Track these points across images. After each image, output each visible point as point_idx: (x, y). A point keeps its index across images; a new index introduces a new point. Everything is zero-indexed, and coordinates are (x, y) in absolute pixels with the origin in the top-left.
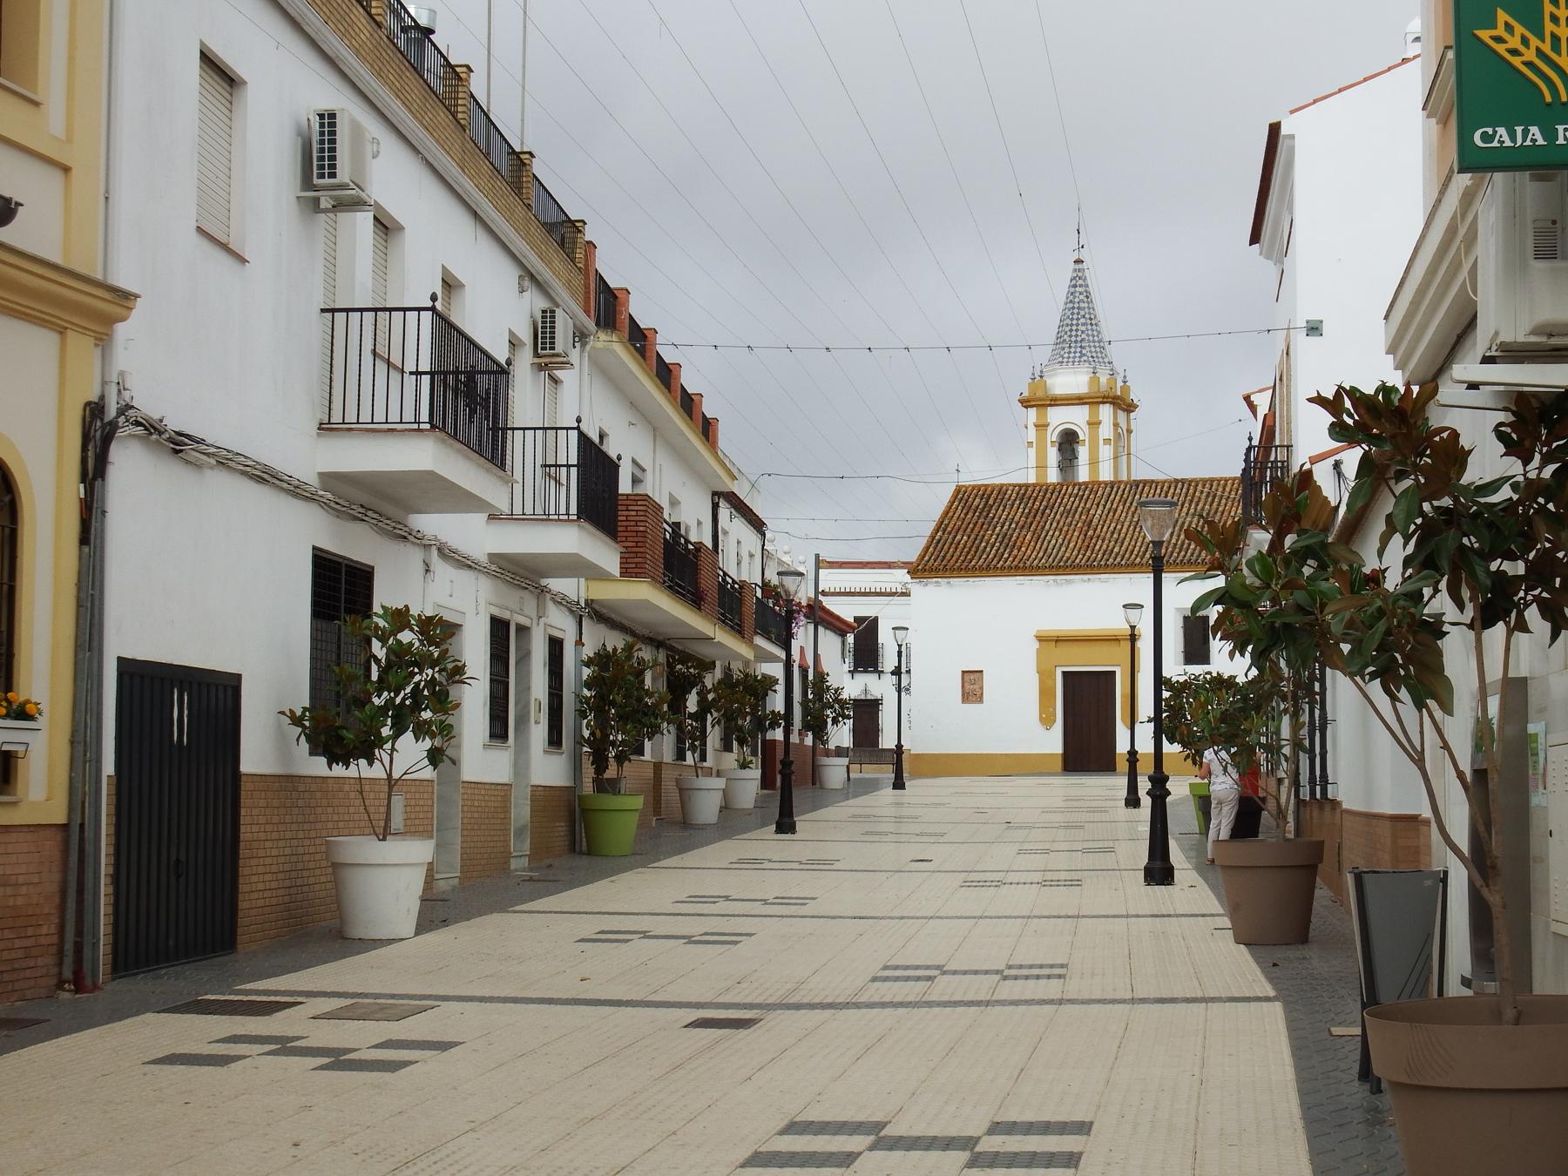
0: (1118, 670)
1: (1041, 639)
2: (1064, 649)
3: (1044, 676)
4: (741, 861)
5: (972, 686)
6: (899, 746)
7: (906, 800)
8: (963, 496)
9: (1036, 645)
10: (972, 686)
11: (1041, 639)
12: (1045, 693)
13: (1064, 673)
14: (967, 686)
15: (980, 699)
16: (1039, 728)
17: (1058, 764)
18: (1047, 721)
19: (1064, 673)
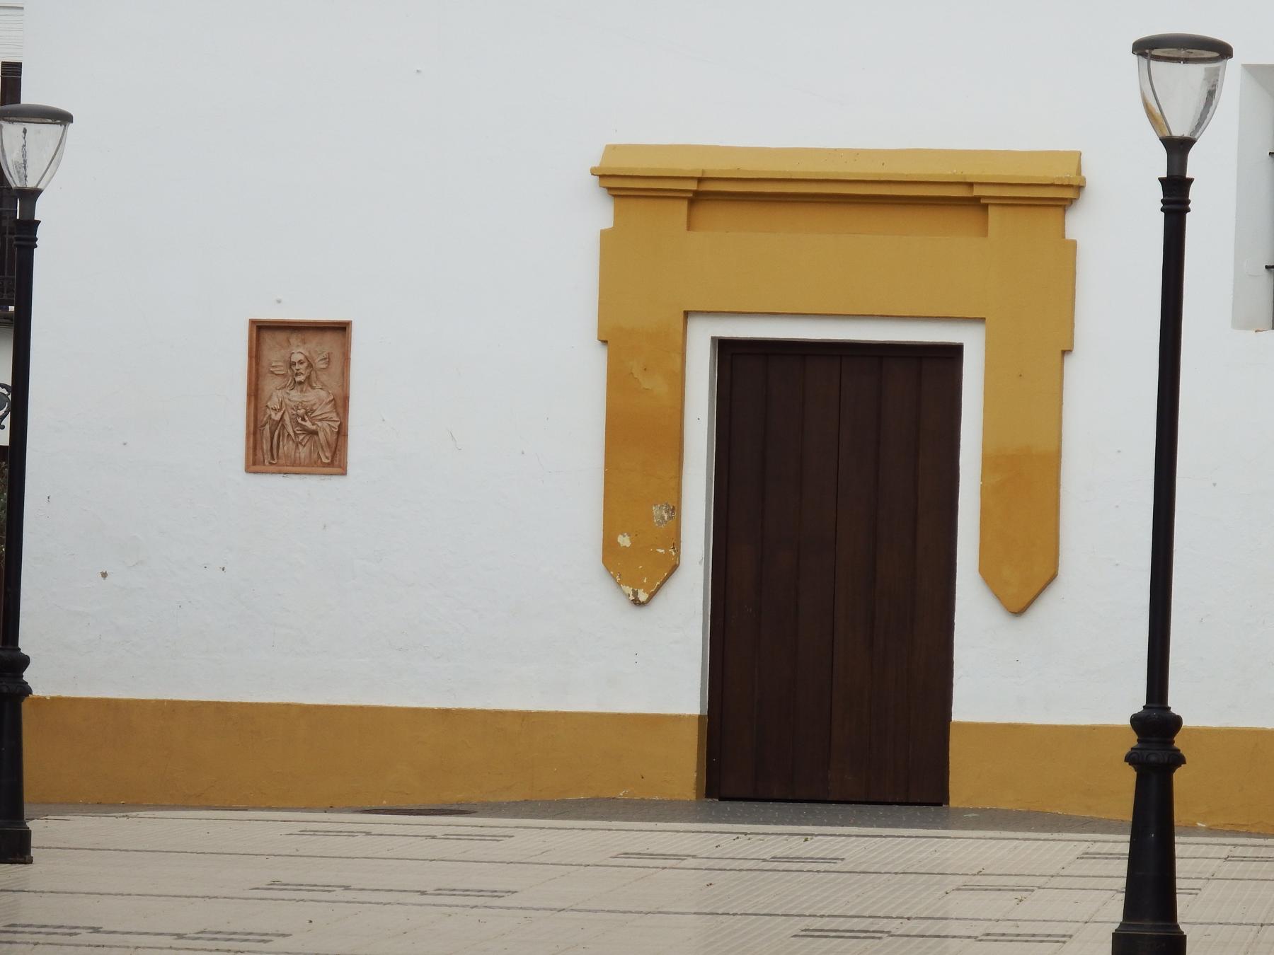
0: (973, 342)
1: (628, 187)
2: (729, 241)
3: (634, 355)
4: (274, 885)
5: (296, 397)
6: (1156, 728)
7: (32, 910)
8: (608, 147)
9: (600, 214)
10: (296, 397)
11: (628, 187)
12: (636, 436)
13: (726, 350)
14: (275, 392)
15: (332, 456)
16: (600, 596)
17: (683, 767)
18: (636, 564)
19: (726, 350)
